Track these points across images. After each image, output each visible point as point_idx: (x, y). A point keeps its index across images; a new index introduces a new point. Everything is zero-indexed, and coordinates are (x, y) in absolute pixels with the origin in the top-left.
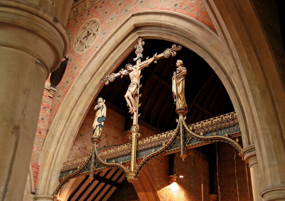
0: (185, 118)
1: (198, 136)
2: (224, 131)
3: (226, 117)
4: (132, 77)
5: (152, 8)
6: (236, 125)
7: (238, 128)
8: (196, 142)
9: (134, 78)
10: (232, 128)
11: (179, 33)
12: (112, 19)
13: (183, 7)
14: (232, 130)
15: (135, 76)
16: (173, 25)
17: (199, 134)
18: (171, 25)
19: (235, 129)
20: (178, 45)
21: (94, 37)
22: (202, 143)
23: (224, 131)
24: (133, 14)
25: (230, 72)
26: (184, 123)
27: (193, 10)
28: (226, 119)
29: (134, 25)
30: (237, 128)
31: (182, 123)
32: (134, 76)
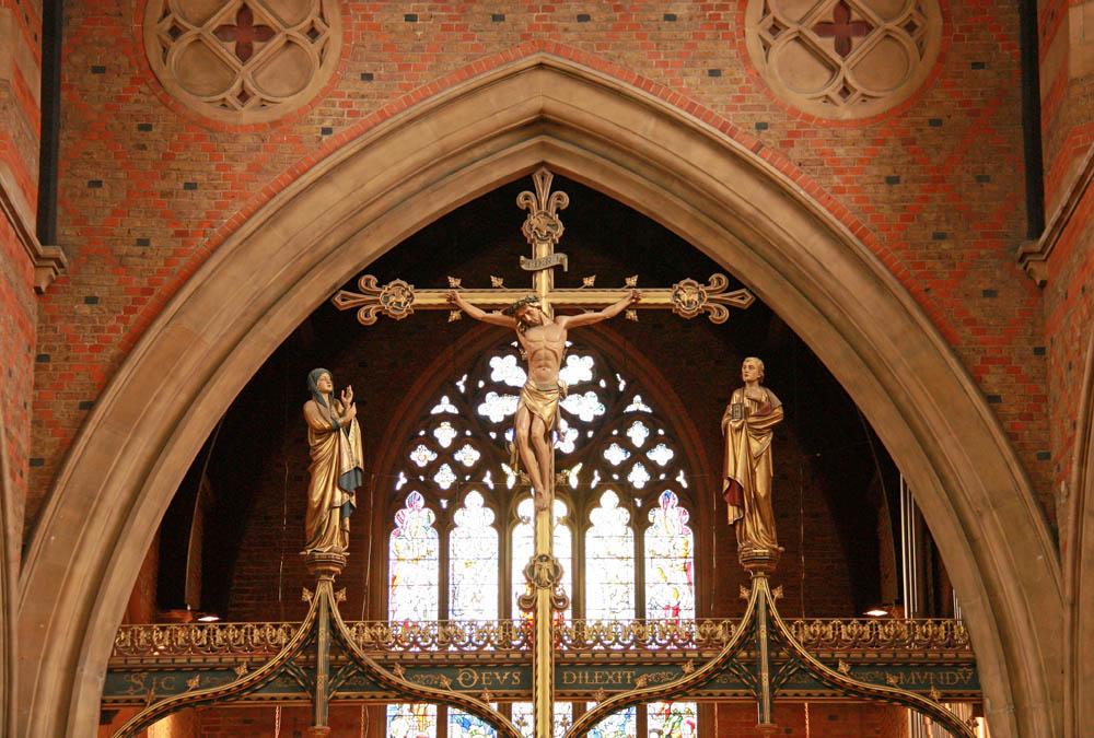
0: (778, 593)
1: (829, 672)
2: (919, 677)
3: (927, 631)
4: (547, 358)
5: (640, 78)
6: (962, 667)
7: (502, 679)
8: (811, 687)
9: (550, 363)
10: (948, 673)
11: (752, 240)
12: (411, 18)
13: (796, 153)
14: (945, 681)
15: (556, 355)
16: (748, 209)
17: (835, 666)
18: (732, 203)
19: (958, 678)
20: (735, 284)
21: (288, 54)
22: (834, 695)
23: (919, 677)
24: (546, 61)
25: (984, 499)
26: (774, 611)
27: (839, 190)
28: (926, 636)
29: (542, 111)
30: (963, 678)
31: (768, 607)
32: (552, 356)
